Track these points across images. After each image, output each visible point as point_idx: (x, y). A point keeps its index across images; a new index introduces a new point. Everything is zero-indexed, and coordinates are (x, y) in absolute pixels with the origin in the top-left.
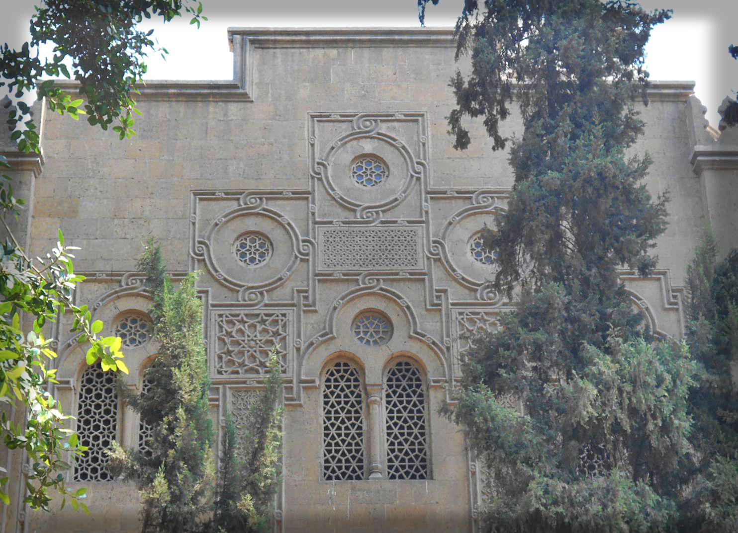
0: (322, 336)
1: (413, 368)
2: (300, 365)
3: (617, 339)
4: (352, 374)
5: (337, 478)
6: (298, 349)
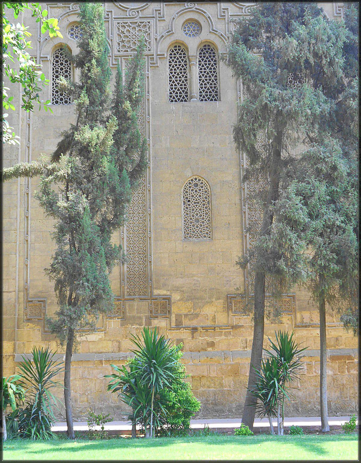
0: (167, 32)
1: (212, 47)
2: (157, 47)
3: (309, 17)
4: (182, 51)
5: (176, 101)
6: (156, 39)
